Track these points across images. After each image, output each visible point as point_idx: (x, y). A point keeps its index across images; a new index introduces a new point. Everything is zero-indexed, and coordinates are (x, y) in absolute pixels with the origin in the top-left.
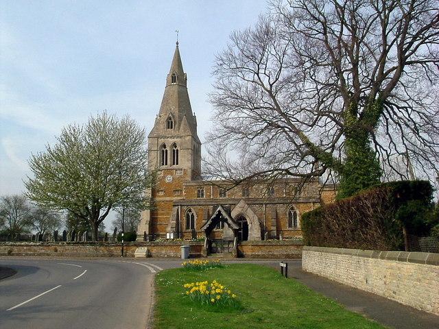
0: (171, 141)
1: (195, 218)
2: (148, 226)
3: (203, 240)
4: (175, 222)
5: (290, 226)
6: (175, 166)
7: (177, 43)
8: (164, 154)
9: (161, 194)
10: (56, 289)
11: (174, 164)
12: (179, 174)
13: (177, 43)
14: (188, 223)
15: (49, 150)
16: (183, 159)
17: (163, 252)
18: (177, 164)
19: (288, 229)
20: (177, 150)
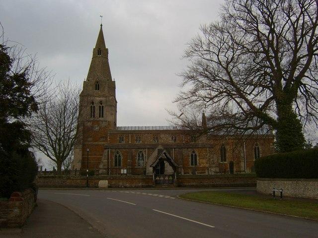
0: (98, 99)
1: (122, 158)
2: (80, 164)
3: (152, 176)
4: (106, 161)
5: (192, 164)
6: (101, 119)
7: (101, 25)
8: (93, 109)
9: (90, 139)
10: (173, 216)
11: (100, 117)
12: (104, 124)
13: (101, 25)
14: (116, 162)
15: (100, 84)
16: (107, 113)
17: (121, 184)
18: (103, 117)
19: (191, 166)
20: (103, 107)
